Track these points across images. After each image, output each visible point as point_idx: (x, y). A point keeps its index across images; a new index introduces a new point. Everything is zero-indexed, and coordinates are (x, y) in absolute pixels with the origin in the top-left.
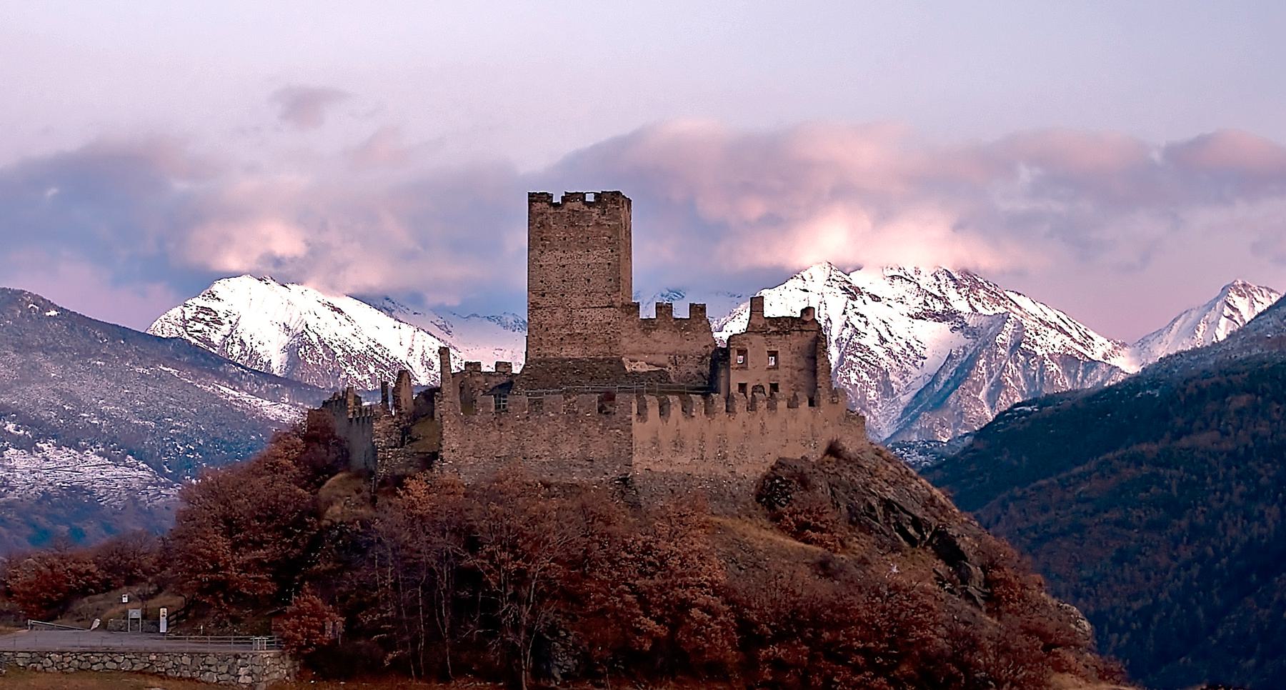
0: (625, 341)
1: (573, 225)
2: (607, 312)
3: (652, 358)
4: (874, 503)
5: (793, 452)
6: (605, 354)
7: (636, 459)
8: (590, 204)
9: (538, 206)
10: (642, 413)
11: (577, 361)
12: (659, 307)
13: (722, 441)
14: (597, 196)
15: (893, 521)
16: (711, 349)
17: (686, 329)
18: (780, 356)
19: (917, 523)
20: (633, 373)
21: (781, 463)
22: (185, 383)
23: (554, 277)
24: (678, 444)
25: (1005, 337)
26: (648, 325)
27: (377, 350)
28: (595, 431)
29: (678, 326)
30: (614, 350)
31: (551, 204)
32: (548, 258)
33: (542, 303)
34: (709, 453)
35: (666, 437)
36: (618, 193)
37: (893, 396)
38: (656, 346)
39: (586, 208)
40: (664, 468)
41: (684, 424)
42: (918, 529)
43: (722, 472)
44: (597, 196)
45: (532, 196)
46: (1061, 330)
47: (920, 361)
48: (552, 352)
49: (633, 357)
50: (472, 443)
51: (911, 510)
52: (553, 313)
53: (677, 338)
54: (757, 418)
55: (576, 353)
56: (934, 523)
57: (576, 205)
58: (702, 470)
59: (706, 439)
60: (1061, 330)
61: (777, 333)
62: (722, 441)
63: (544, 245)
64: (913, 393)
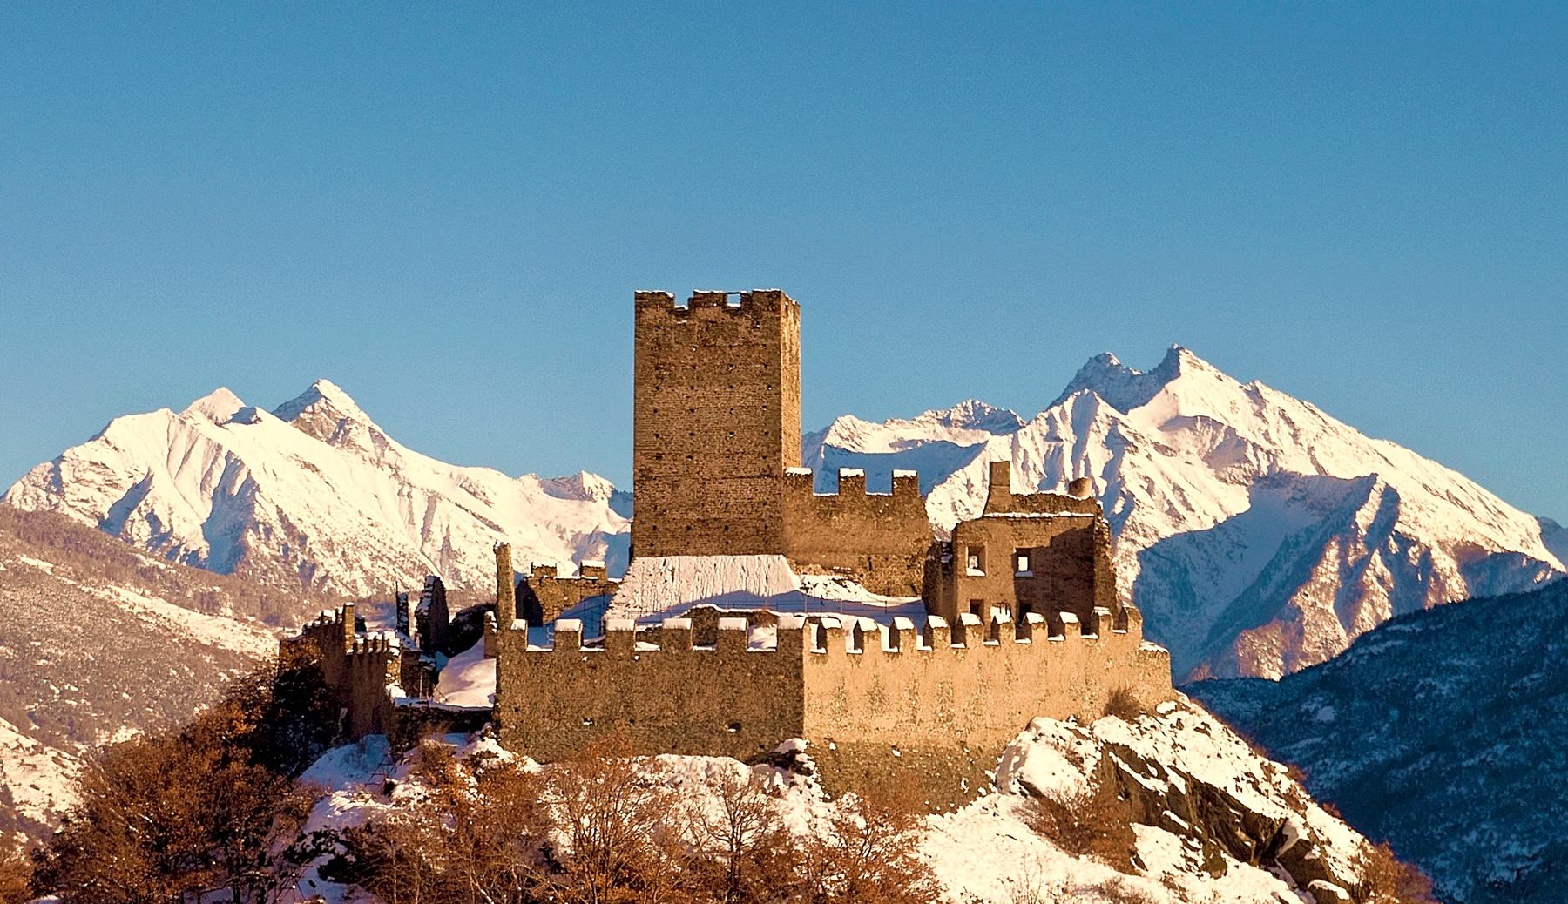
0: (790, 531)
1: (705, 344)
2: (763, 485)
8: (735, 312)
9: (650, 315)
16: (927, 545)
17: (888, 512)
22: (64, 585)
23: (677, 425)
24: (877, 698)
25: (1365, 516)
27: (373, 531)
29: (873, 508)
31: (672, 311)
32: (667, 398)
35: (858, 687)
37: (1195, 606)
38: (838, 539)
43: (945, 740)
44: (746, 299)
45: (638, 297)
46: (1456, 501)
47: (1238, 551)
49: (801, 557)
50: (548, 696)
52: (674, 487)
53: (872, 527)
54: (1001, 655)
57: (713, 313)
58: (914, 737)
59: (921, 690)
60: (1456, 501)
62: (945, 696)
64: (846, 445)
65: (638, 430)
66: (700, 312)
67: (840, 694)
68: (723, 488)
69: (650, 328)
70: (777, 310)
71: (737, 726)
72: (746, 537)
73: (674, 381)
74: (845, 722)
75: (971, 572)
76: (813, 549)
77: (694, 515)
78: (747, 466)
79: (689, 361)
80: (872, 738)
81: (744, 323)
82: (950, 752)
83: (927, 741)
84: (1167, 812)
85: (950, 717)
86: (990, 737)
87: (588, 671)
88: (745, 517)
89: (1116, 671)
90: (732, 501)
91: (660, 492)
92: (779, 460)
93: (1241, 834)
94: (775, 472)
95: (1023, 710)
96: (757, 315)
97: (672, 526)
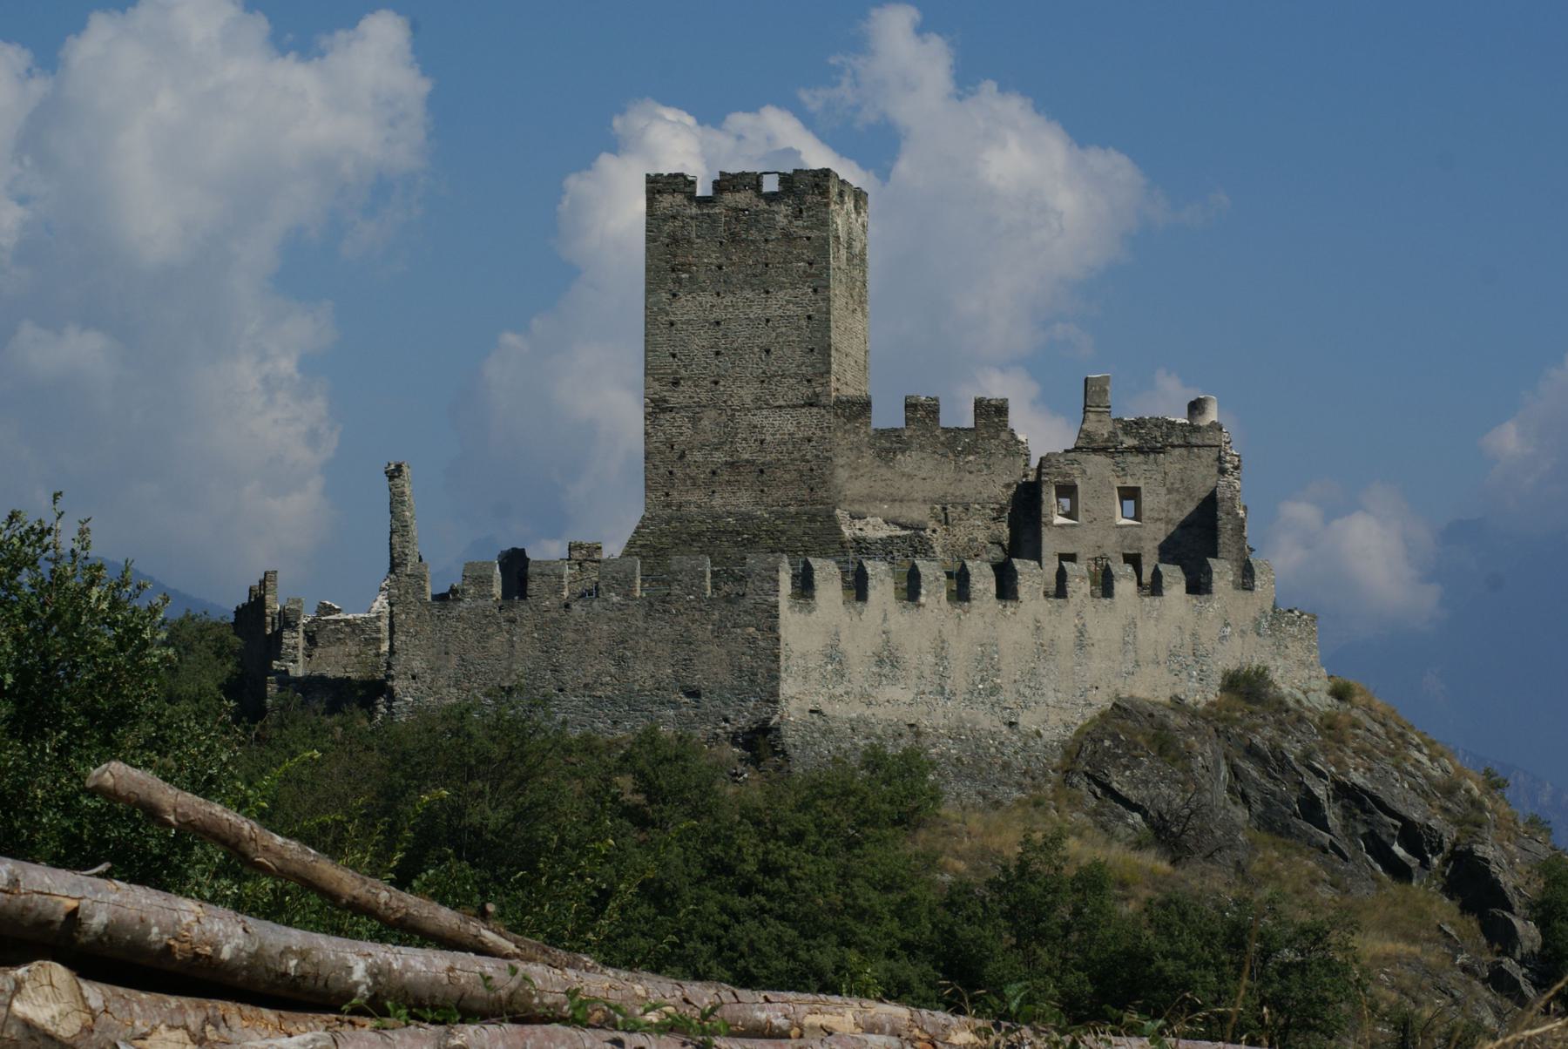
0: (842, 474)
1: (734, 238)
2: (809, 417)
3: (896, 511)
4: (1320, 791)
5: (1151, 686)
6: (801, 502)
7: (787, 688)
8: (771, 198)
9: (666, 201)
10: (805, 585)
11: (745, 518)
12: (911, 406)
13: (987, 662)
14: (785, 179)
15: (1362, 830)
17: (969, 450)
18: (1147, 501)
19: (1412, 835)
20: (857, 541)
21: (1121, 710)
24: (888, 661)
26: (890, 445)
28: (703, 632)
30: (821, 493)
32: (688, 307)
33: (673, 402)
34: (959, 680)
36: (828, 170)
39: (763, 205)
40: (857, 710)
41: (901, 620)
42: (1413, 847)
43: (986, 720)
44: (785, 179)
48: (693, 500)
49: (857, 508)
50: (455, 660)
51: (1400, 808)
52: (695, 420)
53: (948, 470)
55: (743, 501)
56: (1449, 834)
57: (743, 198)
61: (1138, 450)
62: (987, 662)
63: (678, 281)
65: (650, 348)
66: (728, 198)
67: (834, 655)
68: (756, 420)
69: (666, 219)
70: (825, 193)
71: (694, 694)
72: (786, 483)
73: (695, 286)
74: (839, 690)
75: (1059, 520)
76: (872, 498)
77: (720, 457)
78: (790, 391)
79: (714, 258)
80: (880, 712)
81: (782, 213)
82: (993, 735)
83: (961, 719)
84: (114, 773)
85: (995, 690)
86: (1053, 719)
87: (505, 626)
88: (786, 459)
89: (1237, 640)
90: (769, 438)
91: (678, 427)
92: (828, 383)
93: (1398, 850)
94: (823, 400)
95: (1103, 685)
96: (799, 196)
97: (693, 471)
